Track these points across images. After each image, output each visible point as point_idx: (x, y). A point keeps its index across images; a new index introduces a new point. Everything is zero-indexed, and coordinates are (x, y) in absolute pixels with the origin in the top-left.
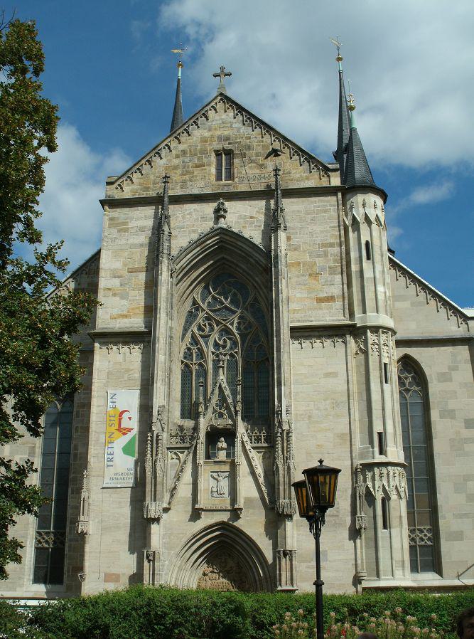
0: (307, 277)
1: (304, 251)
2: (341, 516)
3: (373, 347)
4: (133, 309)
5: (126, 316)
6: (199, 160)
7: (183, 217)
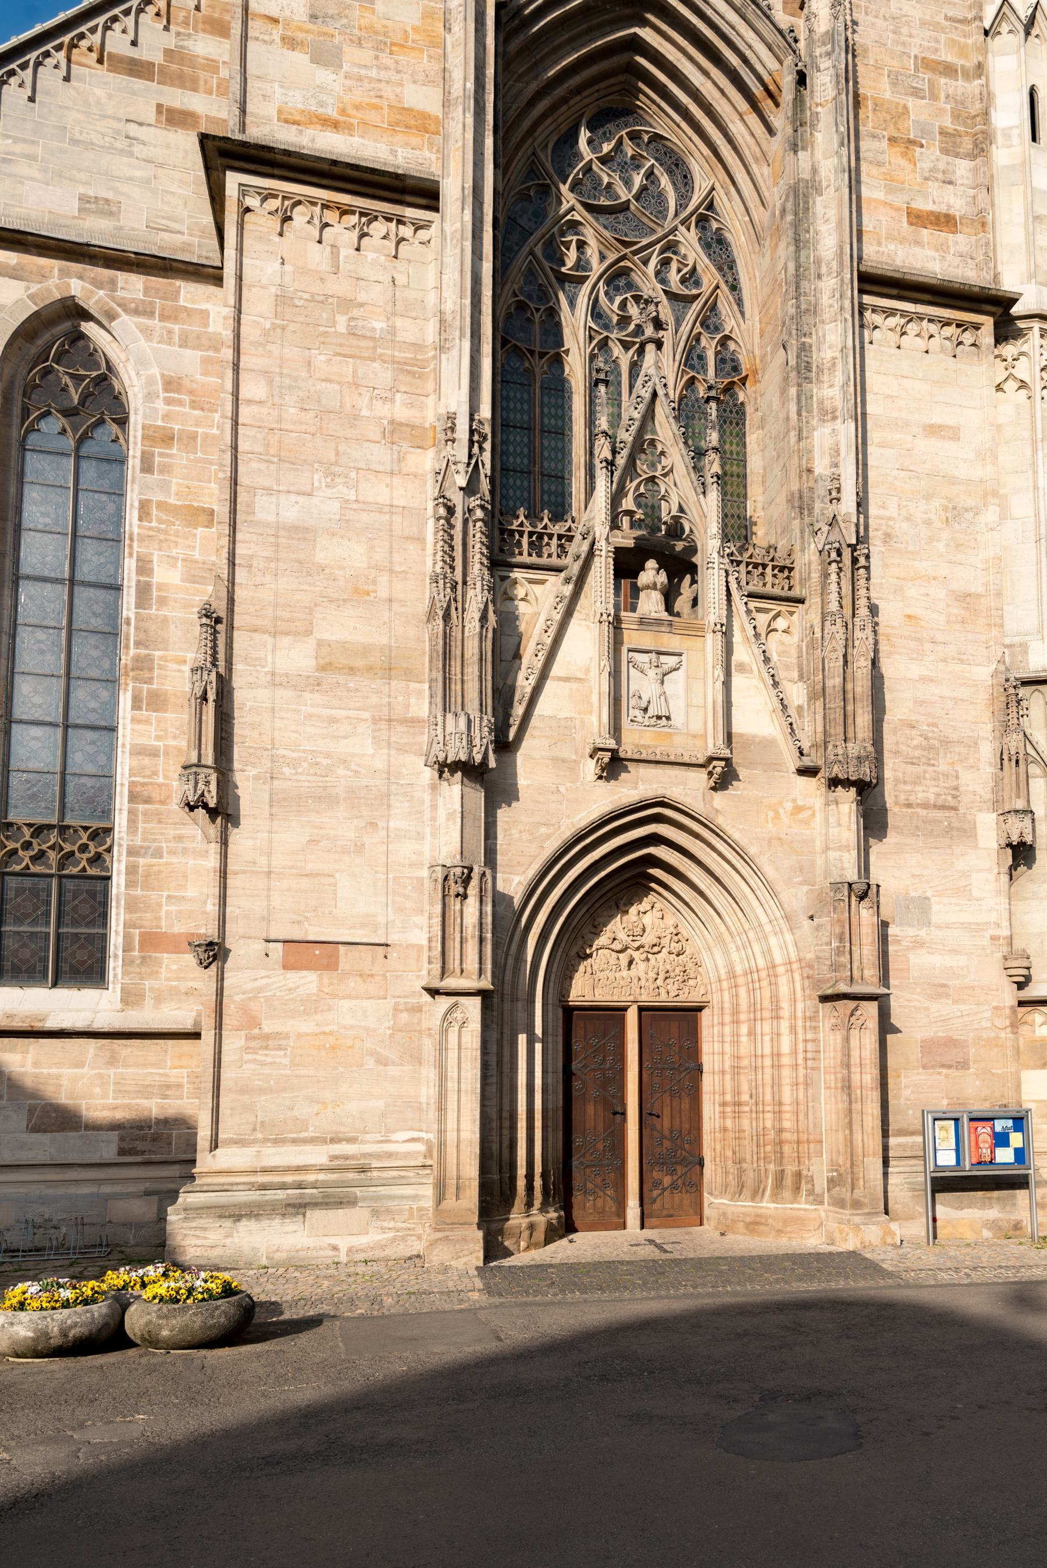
2: (962, 810)
4: (357, 107)
5: (335, 125)
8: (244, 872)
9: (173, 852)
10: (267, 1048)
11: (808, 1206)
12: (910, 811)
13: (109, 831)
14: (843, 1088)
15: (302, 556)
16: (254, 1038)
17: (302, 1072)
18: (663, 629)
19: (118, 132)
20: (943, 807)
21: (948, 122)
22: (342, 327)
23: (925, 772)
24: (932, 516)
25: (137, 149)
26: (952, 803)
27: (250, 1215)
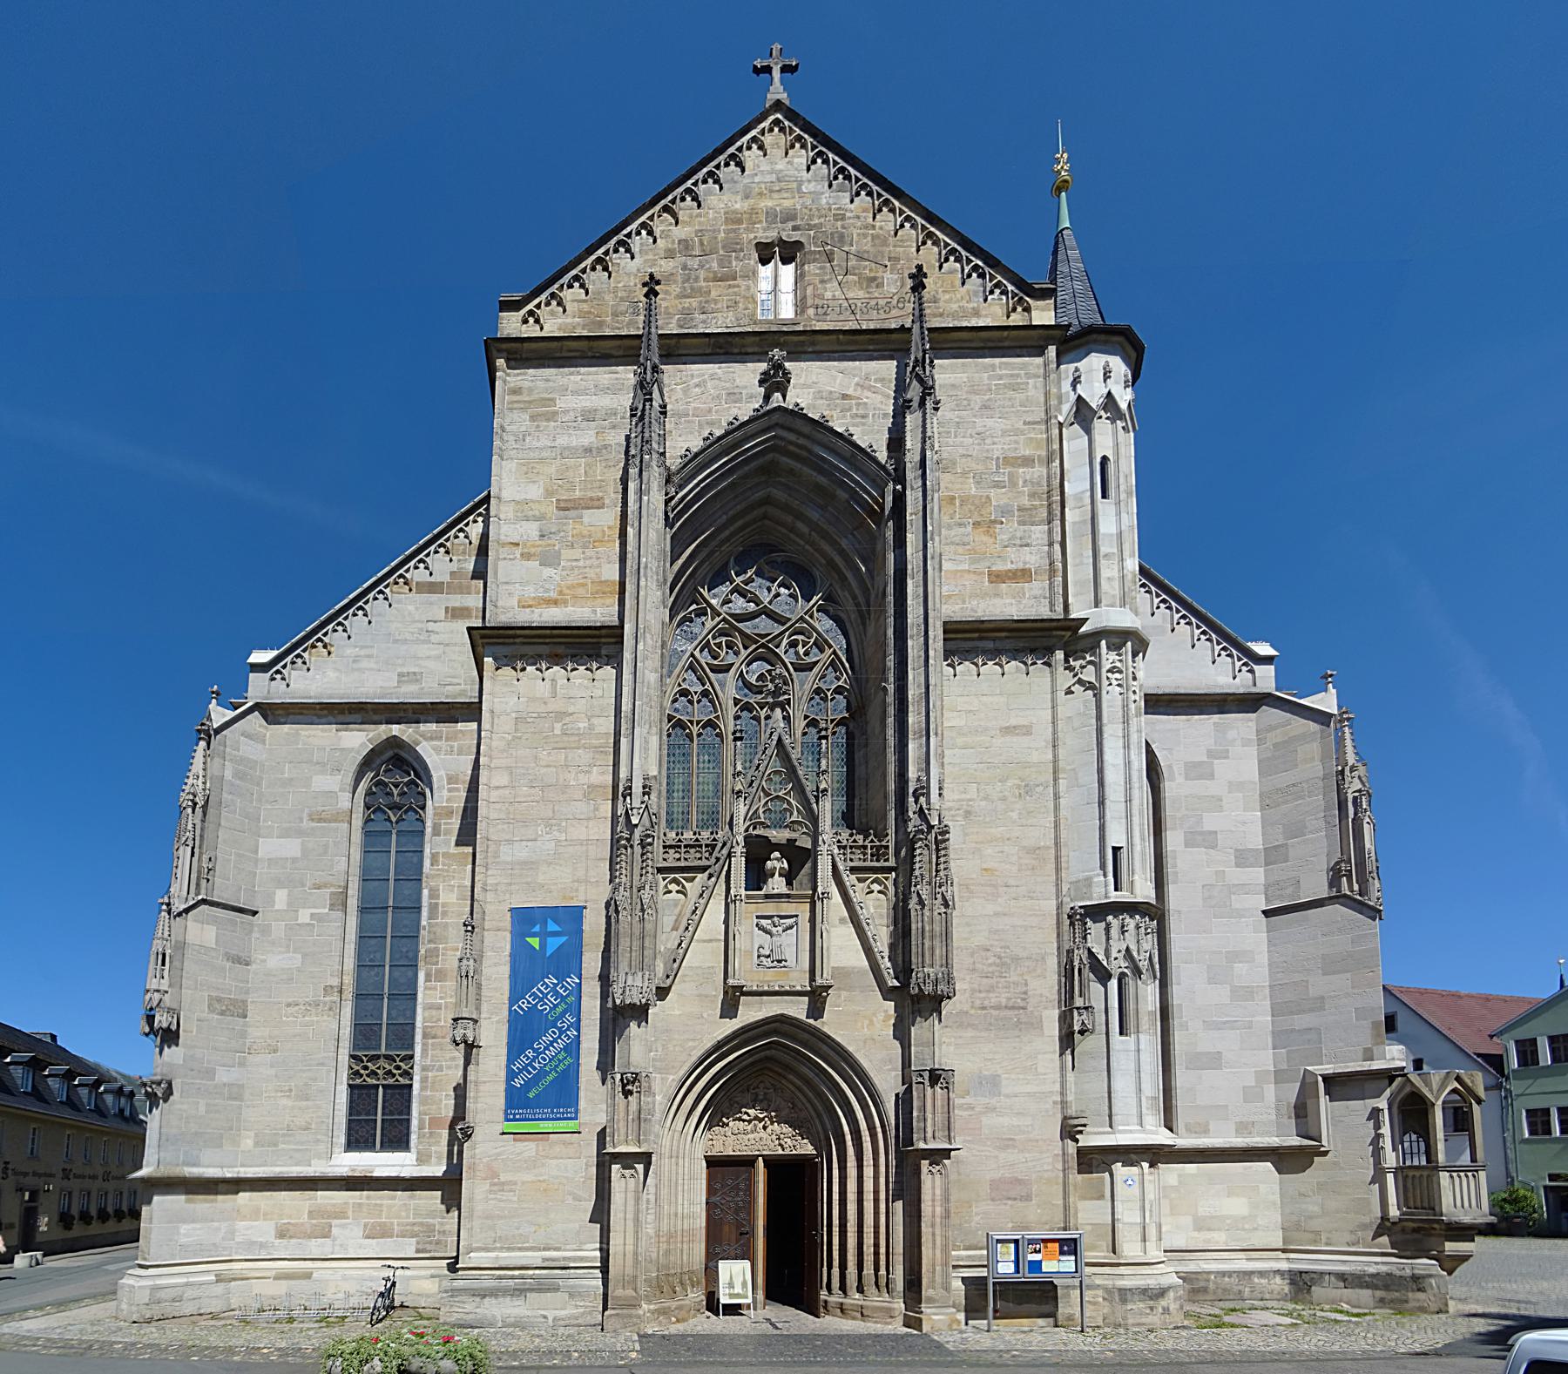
0: (970, 528)
1: (964, 474)
2: (1030, 1009)
3: (1110, 675)
5: (555, 602)
6: (721, 265)
7: (685, 391)
8: (489, 1082)
9: (449, 1068)
10: (503, 1190)
13: (412, 1057)
15: (529, 880)
16: (495, 1184)
17: (525, 1206)
19: (422, 629)
20: (1013, 1008)
21: (1026, 502)
22: (558, 732)
23: (997, 982)
24: (1006, 793)
25: (434, 638)
27: (491, 1295)
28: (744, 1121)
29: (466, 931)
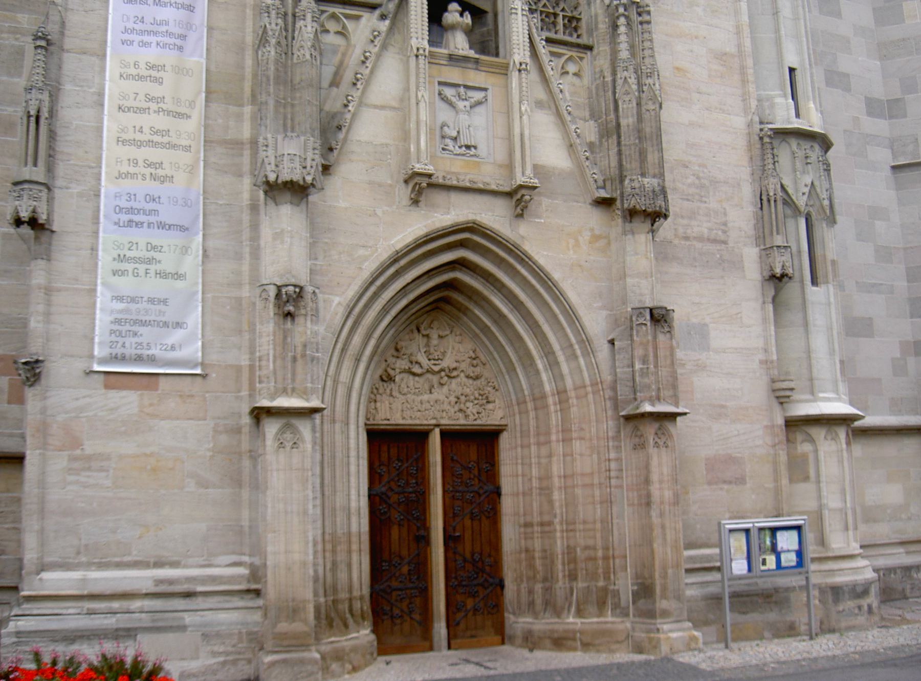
2: (731, 244)
10: (89, 469)
11: (614, 619)
12: (688, 243)
14: (640, 505)
18: (470, 65)
20: (715, 241)
26: (722, 237)
28: (414, 374)
29: (37, 47)
